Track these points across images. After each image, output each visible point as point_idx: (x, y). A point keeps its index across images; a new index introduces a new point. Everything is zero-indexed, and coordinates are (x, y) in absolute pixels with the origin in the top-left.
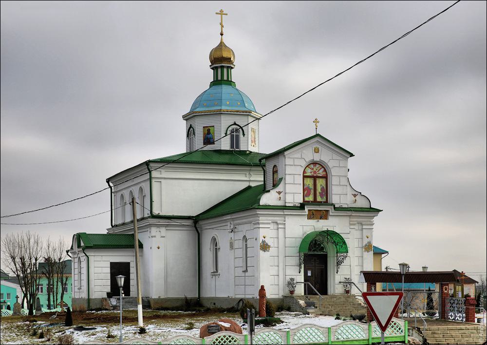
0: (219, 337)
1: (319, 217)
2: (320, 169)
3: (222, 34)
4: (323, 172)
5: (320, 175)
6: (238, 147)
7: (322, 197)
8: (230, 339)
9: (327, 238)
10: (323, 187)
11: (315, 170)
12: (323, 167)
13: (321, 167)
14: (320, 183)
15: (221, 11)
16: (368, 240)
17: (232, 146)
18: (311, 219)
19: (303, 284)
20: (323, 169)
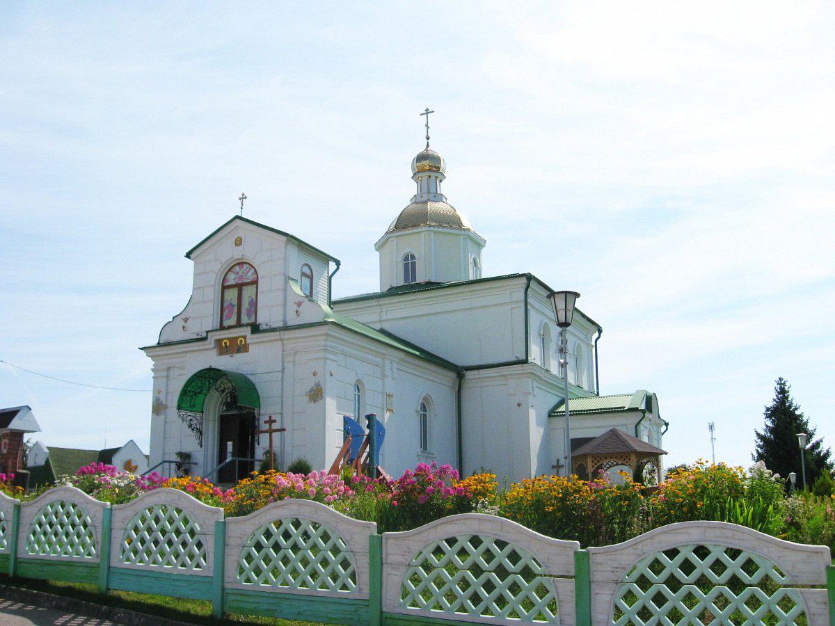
0: (672, 553)
1: (236, 350)
2: (249, 271)
3: (428, 138)
4: (253, 274)
5: (248, 281)
6: (414, 278)
7: (249, 316)
8: (734, 567)
9: (208, 381)
10: (253, 299)
11: (240, 274)
12: (253, 267)
13: (250, 267)
14: (248, 292)
15: (427, 110)
16: (316, 380)
17: (406, 279)
18: (225, 354)
19: (256, 458)
20: (253, 270)
